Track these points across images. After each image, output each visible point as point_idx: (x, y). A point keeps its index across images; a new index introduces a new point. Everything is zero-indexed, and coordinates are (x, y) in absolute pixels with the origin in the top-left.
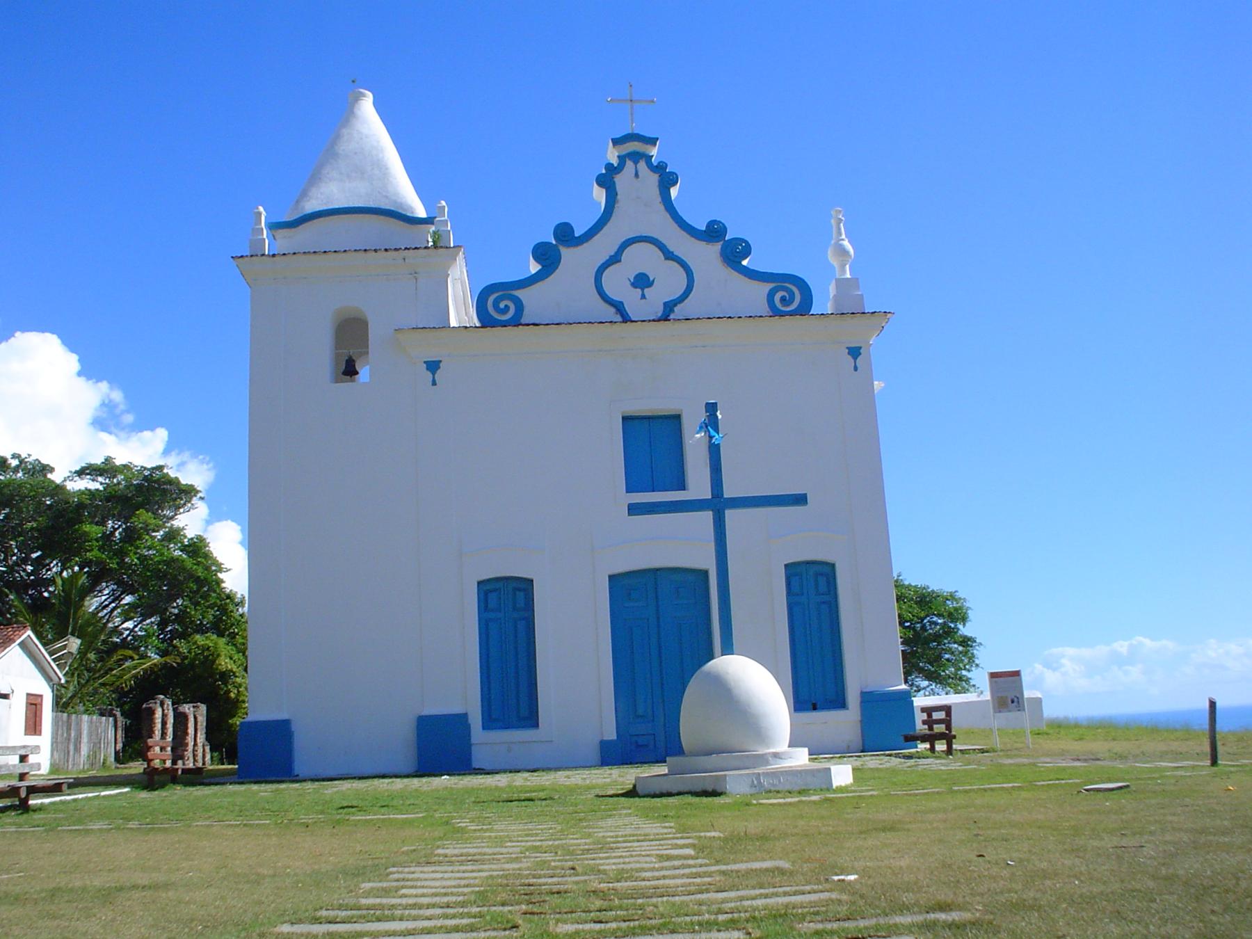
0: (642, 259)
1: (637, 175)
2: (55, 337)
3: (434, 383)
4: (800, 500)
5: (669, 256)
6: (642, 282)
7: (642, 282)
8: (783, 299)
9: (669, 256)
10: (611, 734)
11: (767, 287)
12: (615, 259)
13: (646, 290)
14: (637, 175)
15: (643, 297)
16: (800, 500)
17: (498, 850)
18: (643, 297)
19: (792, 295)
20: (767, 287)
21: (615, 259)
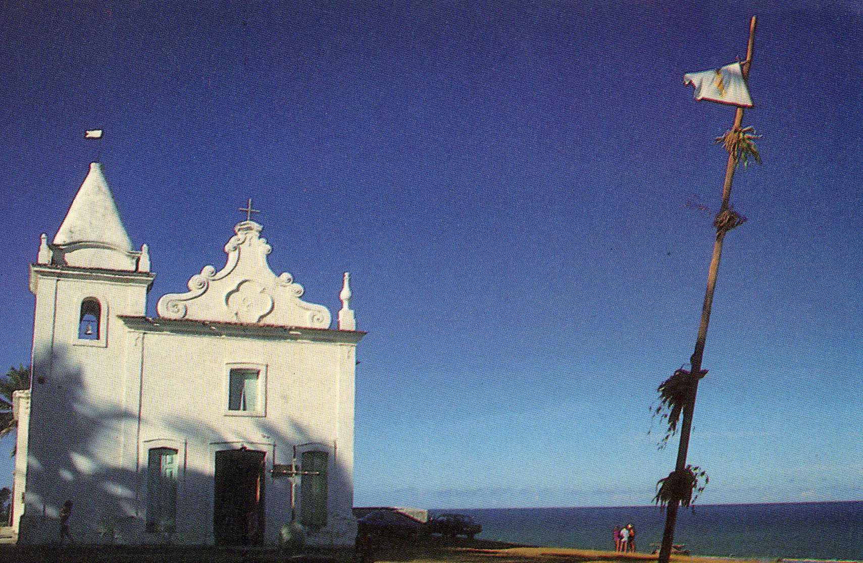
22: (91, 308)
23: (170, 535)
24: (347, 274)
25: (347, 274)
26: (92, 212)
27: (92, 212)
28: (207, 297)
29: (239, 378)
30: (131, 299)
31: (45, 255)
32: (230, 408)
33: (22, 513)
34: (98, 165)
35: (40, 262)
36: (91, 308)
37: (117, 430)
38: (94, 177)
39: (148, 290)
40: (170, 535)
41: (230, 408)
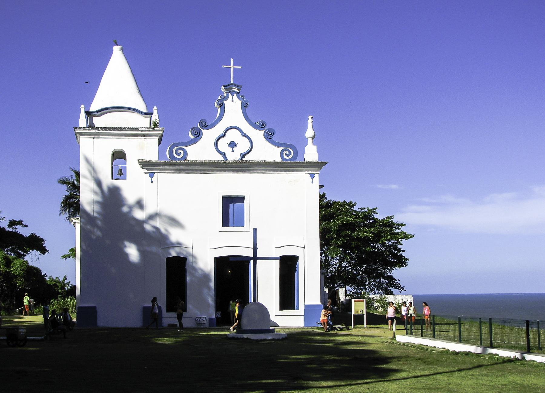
0: (233, 135)
1: (233, 100)
2: (306, 148)
3: (312, 182)
4: (255, 230)
5: (244, 135)
6: (232, 145)
7: (232, 145)
8: (287, 155)
9: (244, 135)
10: (102, 322)
11: (280, 149)
12: (223, 136)
13: (234, 149)
14: (233, 100)
15: (233, 151)
16: (255, 230)
17: (429, 381)
18: (233, 151)
19: (290, 152)
20: (280, 149)
21: (223, 136)
22: (119, 155)
23: (180, 317)
24: (310, 117)
25: (310, 117)
26: (117, 83)
27: (117, 83)
28: (201, 150)
29: (229, 201)
30: (150, 149)
31: (83, 122)
32: (224, 225)
33: (305, 155)
34: (119, 47)
35: (80, 126)
36: (119, 155)
37: (93, 202)
38: (117, 49)
39: (160, 142)
40: (180, 317)
41: (224, 225)
